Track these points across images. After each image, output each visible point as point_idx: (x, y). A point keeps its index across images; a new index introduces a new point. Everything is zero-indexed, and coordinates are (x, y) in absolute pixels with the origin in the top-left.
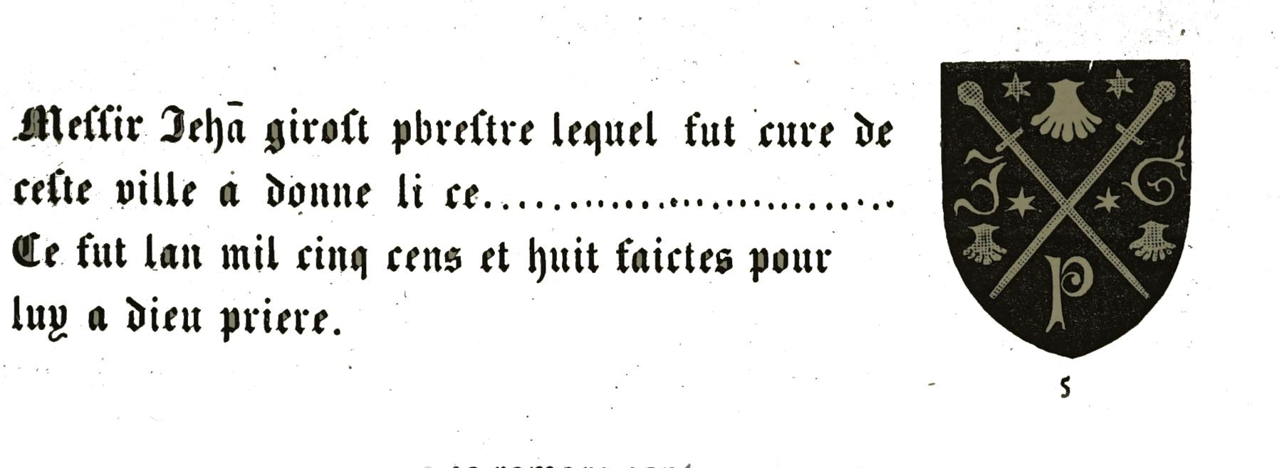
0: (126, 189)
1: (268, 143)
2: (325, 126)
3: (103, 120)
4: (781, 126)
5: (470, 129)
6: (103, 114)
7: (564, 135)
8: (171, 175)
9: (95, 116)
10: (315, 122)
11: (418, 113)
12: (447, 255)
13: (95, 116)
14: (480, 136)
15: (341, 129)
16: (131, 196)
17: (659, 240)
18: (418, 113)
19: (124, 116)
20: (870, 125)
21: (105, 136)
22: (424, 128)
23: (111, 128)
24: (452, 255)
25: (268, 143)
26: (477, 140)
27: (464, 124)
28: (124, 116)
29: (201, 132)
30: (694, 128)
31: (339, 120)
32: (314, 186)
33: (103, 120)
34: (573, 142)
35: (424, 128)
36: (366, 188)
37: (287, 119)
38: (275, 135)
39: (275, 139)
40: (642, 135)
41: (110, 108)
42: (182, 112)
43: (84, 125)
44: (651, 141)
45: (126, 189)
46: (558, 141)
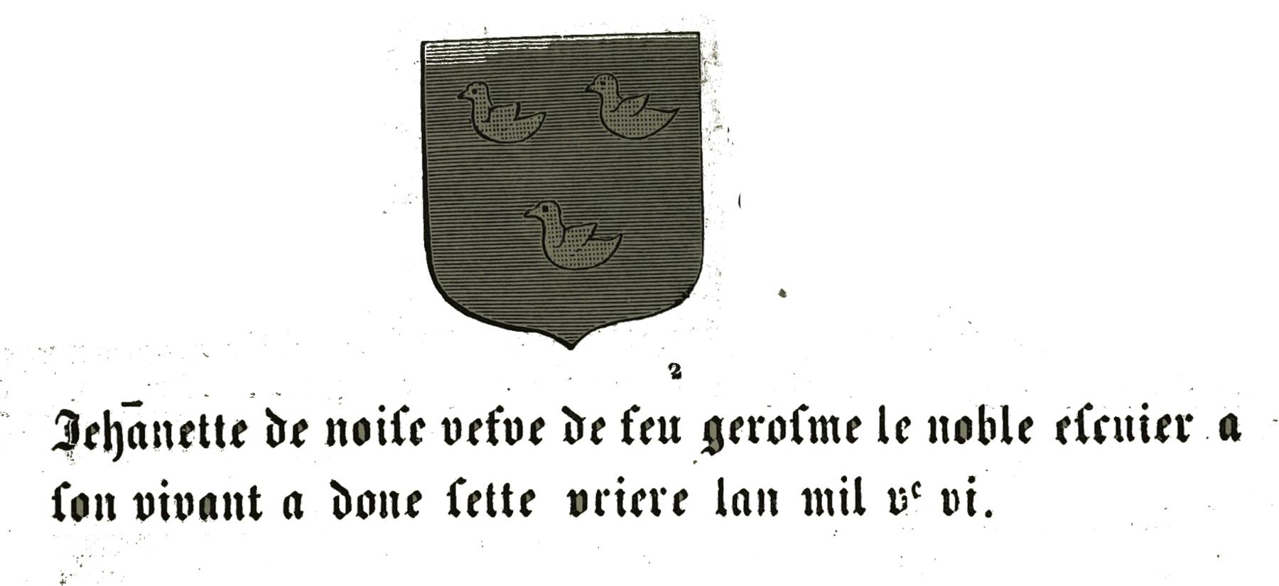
0: (146, 503)
1: (706, 444)
4: (1117, 420)
5: (485, 427)
7: (891, 432)
10: (761, 420)
11: (982, 409)
14: (1086, 434)
16: (152, 510)
17: (1145, 406)
18: (982, 409)
20: (580, 421)
22: (988, 426)
25: (706, 444)
27: (478, 422)
29: (99, 438)
30: (496, 425)
31: (788, 417)
32: (761, 493)
34: (645, 440)
35: (988, 426)
36: (418, 495)
37: (1137, 414)
38: (713, 434)
39: (714, 436)
42: (77, 417)
45: (146, 503)
46: (883, 439)
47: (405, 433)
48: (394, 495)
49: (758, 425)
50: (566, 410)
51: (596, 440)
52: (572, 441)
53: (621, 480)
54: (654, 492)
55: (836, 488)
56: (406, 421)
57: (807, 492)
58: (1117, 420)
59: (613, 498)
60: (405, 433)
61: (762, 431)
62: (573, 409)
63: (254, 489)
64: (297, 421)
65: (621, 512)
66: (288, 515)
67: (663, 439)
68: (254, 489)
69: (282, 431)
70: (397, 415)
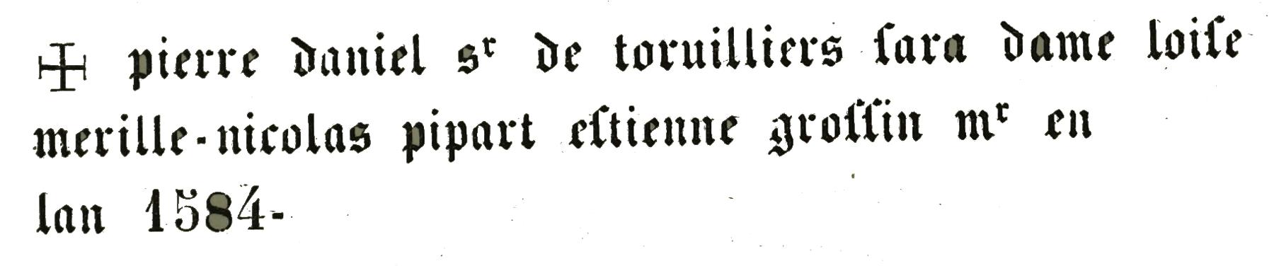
2: (825, 121)
3: (868, 116)
4: (686, 44)
6: (869, 109)
8: (157, 119)
9: (859, 112)
12: (352, 131)
13: (859, 112)
15: (844, 125)
17: (380, 36)
19: (894, 112)
21: (871, 136)
23: (878, 127)
24: (358, 132)
25: (774, 143)
26: (598, 142)
28: (894, 112)
31: (842, 114)
33: (868, 116)
37: (371, 45)
40: (406, 62)
41: (877, 102)
43: (590, 128)
44: (418, 69)
47: (1221, 45)
48: (708, 121)
49: (932, 42)
50: (1004, 25)
51: (571, 67)
52: (303, 73)
53: (250, 115)
54: (99, 133)
55: (117, 125)
56: (1221, 32)
57: (39, 133)
58: (686, 44)
59: (116, 136)
60: (1221, 45)
61: (815, 52)
62: (544, 34)
63: (526, 117)
64: (639, 43)
65: (125, 151)
66: (41, 153)
67: (688, 64)
68: (526, 117)
69: (553, 55)
70: (1211, 26)
